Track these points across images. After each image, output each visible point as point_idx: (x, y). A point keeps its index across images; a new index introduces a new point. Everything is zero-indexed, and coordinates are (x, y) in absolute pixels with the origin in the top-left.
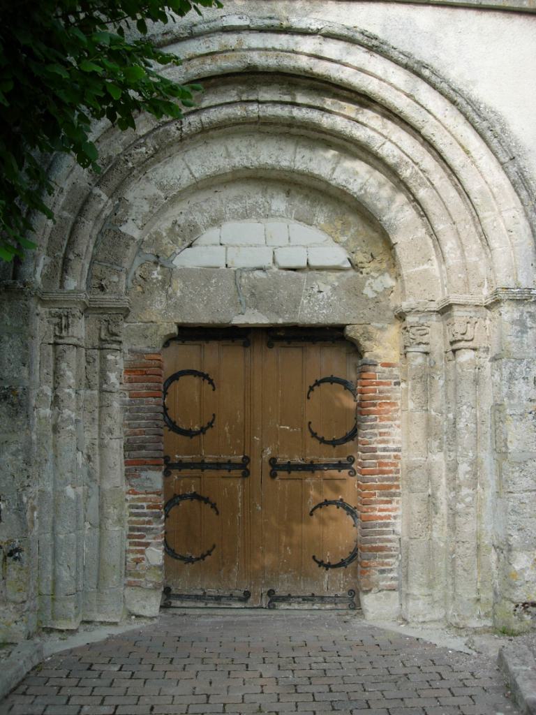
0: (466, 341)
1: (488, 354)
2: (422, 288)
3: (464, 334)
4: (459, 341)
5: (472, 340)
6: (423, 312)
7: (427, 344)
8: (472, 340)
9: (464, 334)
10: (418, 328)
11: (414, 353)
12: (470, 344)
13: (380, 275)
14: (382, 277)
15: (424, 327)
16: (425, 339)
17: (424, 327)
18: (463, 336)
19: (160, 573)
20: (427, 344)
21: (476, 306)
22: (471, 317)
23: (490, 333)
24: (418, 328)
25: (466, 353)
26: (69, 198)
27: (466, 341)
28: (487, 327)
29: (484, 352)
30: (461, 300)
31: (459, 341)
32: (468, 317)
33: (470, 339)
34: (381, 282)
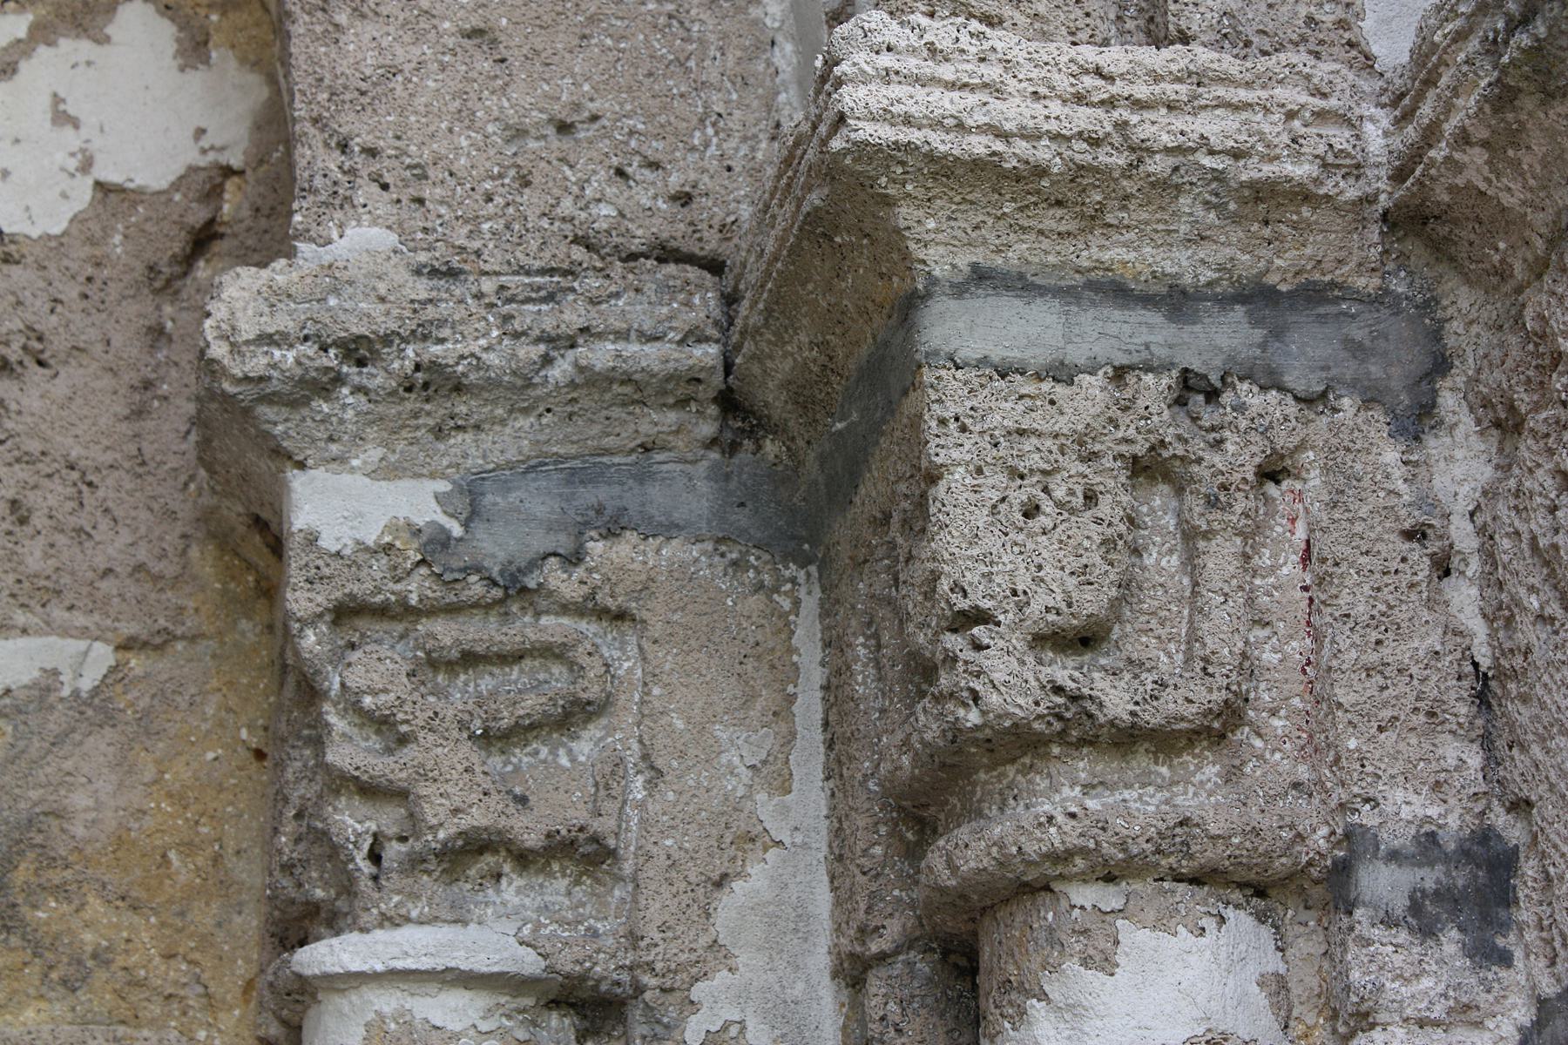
0: (1127, 739)
1: (1489, 955)
2: (524, 99)
3: (1083, 640)
4: (1018, 745)
5: (1219, 728)
6: (519, 390)
7: (584, 853)
8: (1219, 728)
9: (1083, 640)
10: (446, 633)
11: (386, 1001)
12: (1197, 792)
13: (42, 34)
14: (72, 48)
15: (554, 626)
16: (558, 784)
17: (554, 626)
18: (1063, 671)
19: (954, 800)
20: (584, 853)
21: (1260, 192)
22: (1193, 388)
23: (1501, 616)
24: (446, 633)
25: (1134, 938)
26: (1151, 915)
27: (1127, 739)
28: (1462, 534)
29: (1421, 917)
30: (1015, 111)
31: (1018, 745)
32: (1153, 388)
33: (1187, 700)
34: (62, 117)
